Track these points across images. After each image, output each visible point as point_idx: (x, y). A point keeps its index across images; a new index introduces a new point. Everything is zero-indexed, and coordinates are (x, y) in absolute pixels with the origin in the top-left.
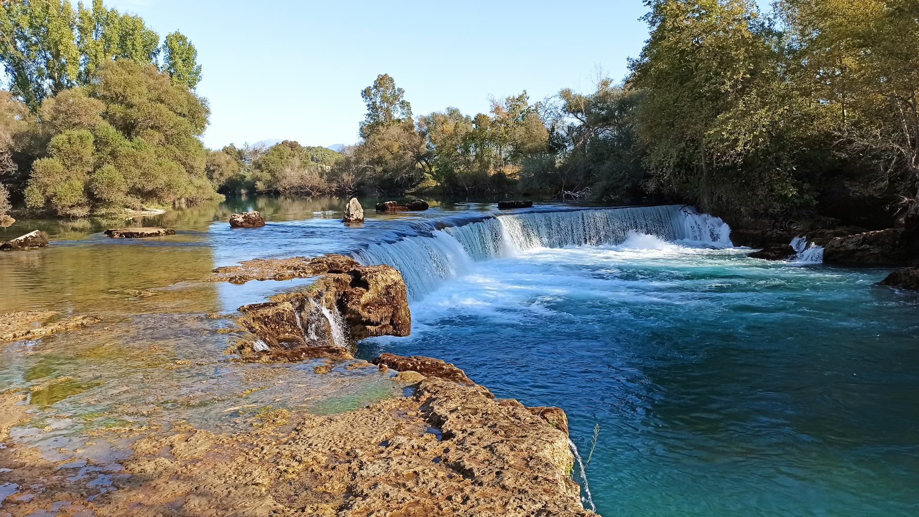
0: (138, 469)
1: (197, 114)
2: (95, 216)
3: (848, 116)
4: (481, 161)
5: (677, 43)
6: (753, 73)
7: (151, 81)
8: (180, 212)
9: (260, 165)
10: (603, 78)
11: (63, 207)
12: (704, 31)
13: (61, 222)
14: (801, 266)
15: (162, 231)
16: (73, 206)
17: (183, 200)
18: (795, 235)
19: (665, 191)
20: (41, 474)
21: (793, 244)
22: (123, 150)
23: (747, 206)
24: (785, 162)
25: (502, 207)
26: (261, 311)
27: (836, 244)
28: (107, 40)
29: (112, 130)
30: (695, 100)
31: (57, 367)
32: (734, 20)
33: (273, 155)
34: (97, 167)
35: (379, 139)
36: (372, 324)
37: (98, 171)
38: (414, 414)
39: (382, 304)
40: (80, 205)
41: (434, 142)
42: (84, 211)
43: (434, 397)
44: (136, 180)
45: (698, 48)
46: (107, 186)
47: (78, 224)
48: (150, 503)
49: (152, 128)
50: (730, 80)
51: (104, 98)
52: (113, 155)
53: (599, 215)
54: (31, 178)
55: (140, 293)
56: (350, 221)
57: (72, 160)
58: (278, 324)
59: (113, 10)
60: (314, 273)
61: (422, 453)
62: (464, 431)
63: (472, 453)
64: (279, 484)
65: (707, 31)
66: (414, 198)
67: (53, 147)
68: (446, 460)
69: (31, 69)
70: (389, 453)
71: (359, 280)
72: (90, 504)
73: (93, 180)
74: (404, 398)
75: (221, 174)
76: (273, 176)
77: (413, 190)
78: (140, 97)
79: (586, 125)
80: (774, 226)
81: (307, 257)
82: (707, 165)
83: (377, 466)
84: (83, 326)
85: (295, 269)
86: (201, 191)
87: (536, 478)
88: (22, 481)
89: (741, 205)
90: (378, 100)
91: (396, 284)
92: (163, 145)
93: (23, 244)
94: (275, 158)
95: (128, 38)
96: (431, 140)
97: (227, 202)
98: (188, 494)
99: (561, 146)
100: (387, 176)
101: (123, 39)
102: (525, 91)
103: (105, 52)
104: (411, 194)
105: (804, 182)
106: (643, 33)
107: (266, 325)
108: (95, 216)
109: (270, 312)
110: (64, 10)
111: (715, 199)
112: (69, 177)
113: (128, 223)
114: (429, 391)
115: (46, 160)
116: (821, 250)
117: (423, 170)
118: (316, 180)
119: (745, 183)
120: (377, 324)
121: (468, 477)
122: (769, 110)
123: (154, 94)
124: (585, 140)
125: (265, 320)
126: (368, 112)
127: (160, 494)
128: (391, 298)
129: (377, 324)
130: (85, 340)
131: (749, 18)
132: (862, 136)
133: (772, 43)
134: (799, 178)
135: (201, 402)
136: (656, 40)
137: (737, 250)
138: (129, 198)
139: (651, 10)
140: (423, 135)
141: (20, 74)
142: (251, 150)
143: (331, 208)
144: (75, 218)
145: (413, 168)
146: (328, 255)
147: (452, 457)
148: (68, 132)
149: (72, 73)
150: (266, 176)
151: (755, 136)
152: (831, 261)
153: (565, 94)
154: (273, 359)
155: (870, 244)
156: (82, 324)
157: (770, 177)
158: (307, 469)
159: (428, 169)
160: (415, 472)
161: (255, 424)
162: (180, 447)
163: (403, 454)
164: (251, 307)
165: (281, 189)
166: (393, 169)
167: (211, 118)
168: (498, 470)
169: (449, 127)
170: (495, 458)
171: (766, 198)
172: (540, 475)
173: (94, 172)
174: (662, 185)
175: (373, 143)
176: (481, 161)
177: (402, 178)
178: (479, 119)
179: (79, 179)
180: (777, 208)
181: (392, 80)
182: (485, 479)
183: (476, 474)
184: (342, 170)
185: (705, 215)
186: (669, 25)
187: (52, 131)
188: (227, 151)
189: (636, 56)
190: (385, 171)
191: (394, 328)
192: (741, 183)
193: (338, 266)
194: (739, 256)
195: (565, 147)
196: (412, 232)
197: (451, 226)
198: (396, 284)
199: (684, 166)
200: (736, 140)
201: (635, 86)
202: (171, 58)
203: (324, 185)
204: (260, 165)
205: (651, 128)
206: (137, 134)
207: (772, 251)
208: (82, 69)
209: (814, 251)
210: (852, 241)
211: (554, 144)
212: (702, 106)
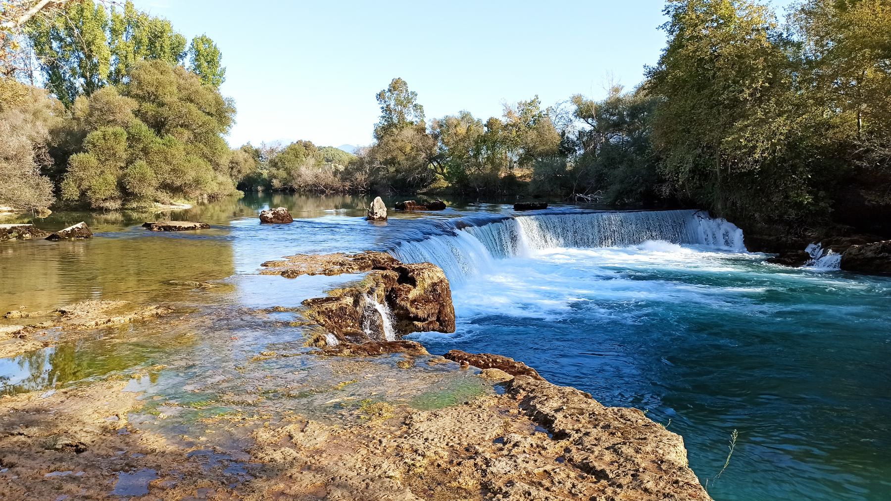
0: (267, 458)
1: (221, 113)
3: (863, 127)
4: (493, 163)
5: (694, 52)
6: (771, 82)
8: (203, 207)
9: (277, 164)
10: (615, 84)
11: (97, 200)
12: (722, 40)
13: (94, 215)
15: (198, 225)
16: (106, 199)
17: (205, 196)
18: (810, 242)
19: (679, 195)
20: (174, 460)
21: (808, 250)
22: (155, 147)
23: (761, 212)
24: (801, 169)
25: (517, 208)
26: (326, 305)
27: (854, 252)
28: (138, 42)
29: (144, 127)
30: (712, 108)
31: (149, 355)
32: (752, 30)
34: (130, 162)
35: (393, 141)
37: (130, 167)
38: (516, 411)
39: (428, 301)
40: (112, 198)
41: (447, 144)
42: (116, 205)
43: (532, 395)
44: (166, 176)
45: (716, 57)
46: (139, 181)
47: (111, 216)
48: (293, 493)
49: (181, 126)
50: (748, 89)
51: (137, 97)
52: (145, 151)
53: (616, 217)
54: (67, 172)
55: (201, 285)
56: (374, 219)
57: (106, 155)
58: (341, 318)
59: (143, 14)
60: (360, 269)
61: (543, 452)
62: (578, 431)
63: (596, 453)
64: (410, 478)
65: (726, 40)
66: (425, 197)
67: (88, 142)
68: (571, 460)
69: (65, 69)
70: (510, 451)
71: (406, 277)
72: (235, 493)
73: (125, 175)
74: (499, 396)
75: (239, 172)
76: (289, 174)
77: (425, 190)
78: (171, 97)
79: (597, 130)
80: (789, 233)
81: (347, 253)
82: (721, 171)
83: (504, 463)
84: (158, 316)
85: (341, 265)
86: (222, 187)
87: (677, 482)
88: (159, 467)
89: (756, 211)
90: (392, 103)
91: (441, 281)
92: (192, 142)
93: (70, 235)
95: (156, 42)
97: (244, 199)
98: (326, 485)
99: (571, 150)
100: (400, 176)
101: (152, 43)
102: (537, 96)
103: (135, 52)
104: (423, 194)
105: (819, 190)
106: (661, 41)
107: (330, 319)
109: (334, 306)
110: (97, 16)
111: (729, 204)
112: (102, 172)
113: (158, 216)
114: (524, 390)
115: (81, 155)
116: (839, 257)
117: (434, 171)
118: (330, 179)
120: (424, 320)
121: (601, 478)
122: (787, 119)
123: (184, 93)
124: (596, 145)
125: (329, 314)
126: (382, 114)
127: (299, 484)
128: (438, 295)
129: (424, 320)
130: (164, 329)
131: (767, 28)
132: (882, 145)
133: (789, 52)
134: (814, 186)
135: (300, 393)
136: (674, 48)
137: (748, 256)
138: (159, 193)
140: (436, 137)
141: (54, 73)
142: (268, 148)
143: (344, 206)
144: (107, 210)
145: (425, 169)
146: (368, 252)
147: (578, 457)
149: (104, 72)
153: (577, 100)
154: (354, 352)
156: (157, 314)
157: (786, 184)
158: (432, 464)
159: (439, 170)
160: (545, 471)
161: (362, 416)
162: (299, 437)
163: (524, 452)
164: (314, 301)
165: (296, 187)
166: (406, 171)
167: (237, 117)
168: (632, 472)
169: (462, 130)
170: (622, 460)
171: (781, 205)
172: (680, 479)
174: (676, 190)
175: (386, 144)
176: (493, 163)
177: (414, 179)
178: (490, 124)
179: (112, 174)
180: (792, 214)
181: (405, 84)
182: (624, 481)
183: (611, 476)
184: (358, 169)
185: (719, 220)
186: (688, 33)
187: (88, 128)
188: (245, 150)
189: (654, 63)
190: (397, 171)
191: (441, 325)
193: (380, 262)
195: (575, 151)
196: (438, 231)
197: (471, 226)
198: (441, 281)
199: (700, 172)
200: (755, 147)
201: (650, 92)
202: (196, 60)
203: (337, 183)
204: (277, 164)
206: (168, 131)
207: (789, 257)
208: (112, 69)
209: (832, 257)
210: (870, 249)
211: (564, 147)
212: (719, 114)
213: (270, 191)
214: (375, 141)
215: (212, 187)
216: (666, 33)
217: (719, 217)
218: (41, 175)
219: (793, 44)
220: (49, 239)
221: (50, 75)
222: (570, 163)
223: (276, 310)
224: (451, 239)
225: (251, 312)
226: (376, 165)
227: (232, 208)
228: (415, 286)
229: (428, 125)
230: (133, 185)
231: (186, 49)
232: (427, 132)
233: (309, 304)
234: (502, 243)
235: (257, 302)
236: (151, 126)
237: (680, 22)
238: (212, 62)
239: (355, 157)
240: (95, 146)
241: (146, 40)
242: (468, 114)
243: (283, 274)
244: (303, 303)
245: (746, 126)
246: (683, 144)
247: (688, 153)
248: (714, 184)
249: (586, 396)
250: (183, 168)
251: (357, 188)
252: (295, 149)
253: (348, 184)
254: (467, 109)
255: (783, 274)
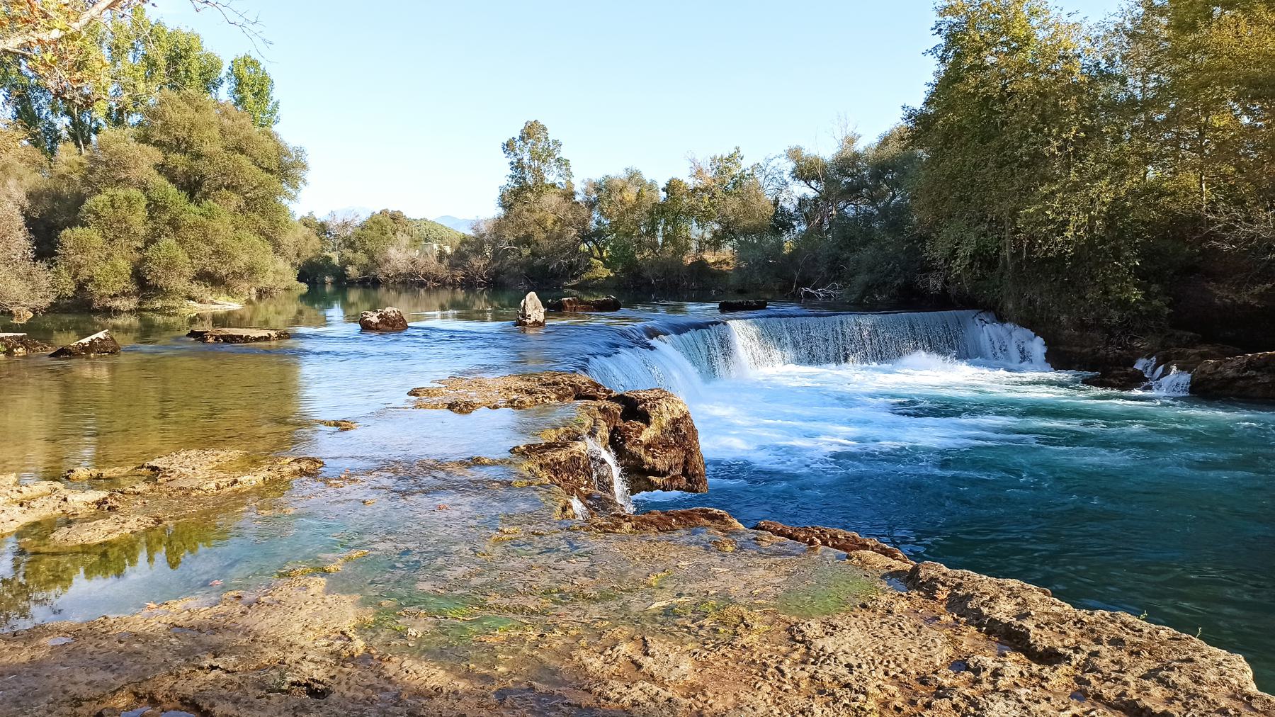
1: (285, 168)
2: (144, 310)
7: (226, 122)
10: (850, 130)
11: (101, 296)
13: (96, 319)
14: (1161, 400)
16: (115, 295)
19: (952, 290)
21: (1139, 365)
27: (1208, 369)
28: (152, 64)
29: (172, 189)
33: (371, 229)
34: (151, 241)
36: (658, 474)
39: (667, 446)
40: (124, 294)
42: (131, 303)
44: (206, 261)
45: (1009, 95)
46: (166, 268)
49: (227, 188)
50: (1057, 140)
51: (159, 144)
52: (174, 224)
54: (57, 255)
56: (525, 324)
57: (115, 230)
59: (158, 23)
61: (1044, 684)
76: (371, 258)
77: (575, 282)
78: (211, 145)
79: (825, 197)
80: (1108, 343)
82: (1013, 256)
86: (278, 278)
90: (526, 158)
94: (374, 233)
95: (179, 63)
96: (602, 214)
97: (303, 297)
102: (737, 148)
104: (572, 287)
106: (928, 71)
108: (144, 310)
109: (562, 455)
111: (1023, 303)
112: (109, 255)
113: (192, 321)
114: (943, 584)
115: (78, 230)
116: (1186, 378)
119: (1069, 282)
123: (231, 139)
125: (555, 468)
126: (511, 172)
134: (1144, 277)
137: (1052, 375)
138: (195, 286)
139: (942, 41)
140: (591, 205)
142: (339, 221)
143: (454, 305)
144: (117, 312)
145: (576, 251)
148: (110, 191)
150: (361, 257)
151: (1091, 217)
152: (1202, 392)
153: (794, 154)
155: (1258, 369)
156: (301, 470)
157: (1105, 275)
159: (597, 253)
165: (383, 277)
167: (308, 176)
173: (146, 248)
175: (518, 216)
176: (674, 243)
177: (560, 265)
178: (671, 188)
179: (124, 258)
180: (1115, 316)
181: (544, 129)
185: (1009, 326)
187: (85, 190)
189: (918, 103)
190: (533, 254)
191: (689, 480)
192: (1062, 281)
194: (1061, 385)
196: (625, 341)
197: (667, 334)
199: (986, 260)
200: (1065, 223)
202: (238, 92)
203: (443, 271)
205: (935, 202)
206: (206, 196)
207: (1115, 377)
209: (1177, 377)
210: (1232, 366)
213: (343, 283)
214: (501, 211)
215: (267, 281)
216: (937, 61)
217: (1010, 321)
218: (35, 260)
219: (1116, 77)
220: (55, 355)
221: (18, 112)
222: (788, 241)
223: (476, 462)
224: (646, 352)
225: (440, 465)
226: (504, 245)
227: (293, 308)
228: (648, 424)
229: (579, 187)
230: (154, 273)
231: (223, 75)
232: (578, 198)
233: (523, 453)
234: (713, 357)
235: (440, 450)
236: (181, 187)
237: (959, 46)
238: (261, 94)
239: (470, 233)
240: (98, 217)
241: (162, 62)
242: (638, 173)
243: (451, 407)
244: (512, 451)
245: (1053, 193)
246: (961, 217)
247: (969, 230)
248: (1002, 274)
249: (1045, 593)
250: (230, 250)
251: (474, 279)
252: (378, 223)
253: (460, 272)
254: (637, 166)
255: (1089, 397)
